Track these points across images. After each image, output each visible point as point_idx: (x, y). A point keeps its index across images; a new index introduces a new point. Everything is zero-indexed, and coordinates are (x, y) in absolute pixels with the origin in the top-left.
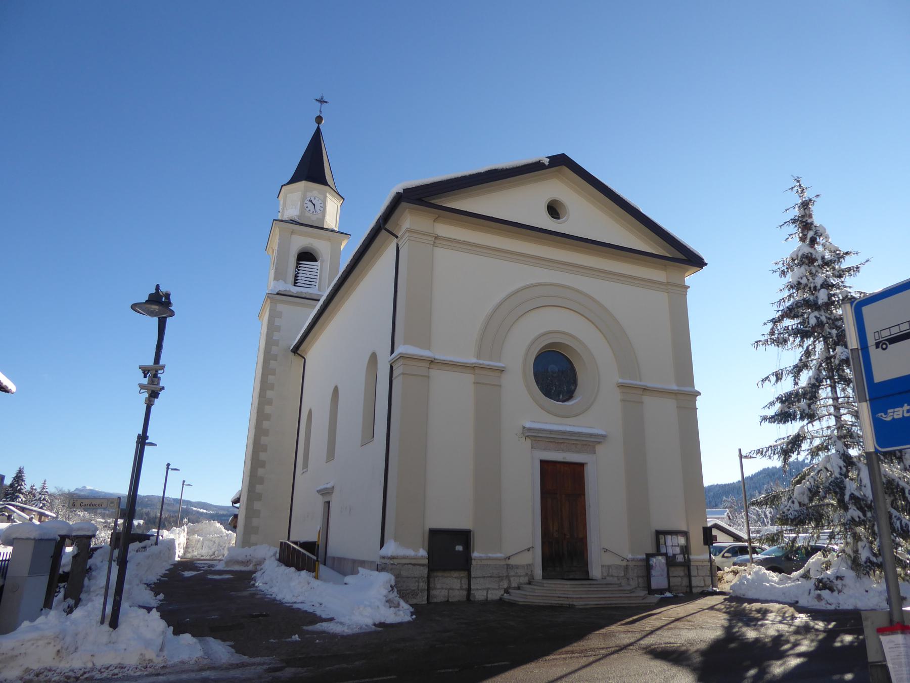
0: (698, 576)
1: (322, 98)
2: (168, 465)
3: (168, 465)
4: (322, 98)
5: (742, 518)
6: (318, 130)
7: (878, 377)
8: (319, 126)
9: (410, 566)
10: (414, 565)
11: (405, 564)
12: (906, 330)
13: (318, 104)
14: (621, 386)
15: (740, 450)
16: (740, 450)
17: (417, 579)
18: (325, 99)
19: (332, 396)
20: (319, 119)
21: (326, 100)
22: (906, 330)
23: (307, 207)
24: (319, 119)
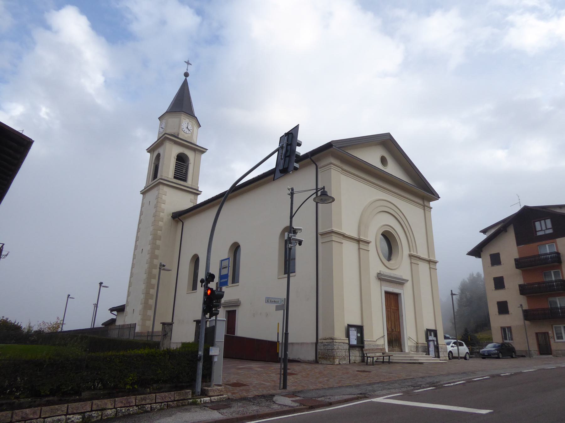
0: (443, 352)
1: (188, 61)
2: (69, 295)
3: (69, 295)
4: (188, 61)
5: (149, 397)
6: (186, 80)
7: (209, 317)
8: (186, 79)
9: (342, 344)
10: (343, 343)
11: (340, 342)
12: (92, 321)
13: (186, 64)
14: (322, 243)
15: (451, 291)
16: (451, 291)
17: (345, 351)
18: (190, 62)
19: (282, 232)
20: (186, 75)
21: (186, 63)
22: (92, 321)
23: (183, 128)
24: (186, 75)
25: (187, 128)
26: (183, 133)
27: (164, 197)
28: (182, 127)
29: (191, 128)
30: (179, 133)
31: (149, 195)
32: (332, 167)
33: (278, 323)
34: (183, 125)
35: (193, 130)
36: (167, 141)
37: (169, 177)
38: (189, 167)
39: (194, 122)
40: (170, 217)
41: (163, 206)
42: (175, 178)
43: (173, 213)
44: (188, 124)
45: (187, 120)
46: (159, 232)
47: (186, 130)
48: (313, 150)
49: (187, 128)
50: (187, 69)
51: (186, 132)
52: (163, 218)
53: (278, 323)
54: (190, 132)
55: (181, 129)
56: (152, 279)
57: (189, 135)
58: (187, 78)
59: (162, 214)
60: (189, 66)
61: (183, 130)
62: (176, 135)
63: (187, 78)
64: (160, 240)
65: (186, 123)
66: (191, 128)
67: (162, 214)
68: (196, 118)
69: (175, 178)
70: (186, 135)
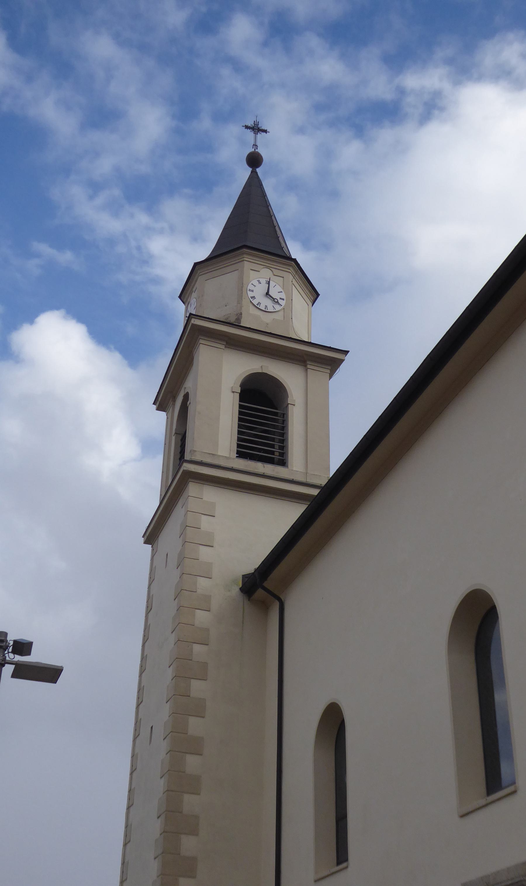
23: (253, 297)
25: (267, 294)
26: (253, 311)
27: (205, 522)
28: (250, 294)
29: (283, 295)
30: (241, 314)
31: (259, 270)
32: (245, 259)
33: (279, 292)
34: (250, 287)
35: (290, 300)
36: (201, 341)
37: (219, 453)
38: (287, 439)
39: (290, 277)
40: (236, 590)
41: (204, 553)
42: (241, 455)
43: (244, 576)
44: (269, 283)
45: (266, 273)
46: (197, 648)
47: (266, 303)
48: (468, 308)
49: (267, 294)
50: (255, 145)
51: (266, 307)
52: (207, 598)
53: (279, 292)
54: (278, 307)
55: (245, 302)
56: (183, 836)
57: (279, 317)
58: (258, 170)
59: (203, 583)
60: (260, 136)
61: (255, 302)
62: (232, 320)
63: (258, 170)
64: (204, 679)
65: (263, 281)
66: (283, 295)
67: (203, 583)
68: (295, 261)
69: (241, 455)
70: (267, 318)
